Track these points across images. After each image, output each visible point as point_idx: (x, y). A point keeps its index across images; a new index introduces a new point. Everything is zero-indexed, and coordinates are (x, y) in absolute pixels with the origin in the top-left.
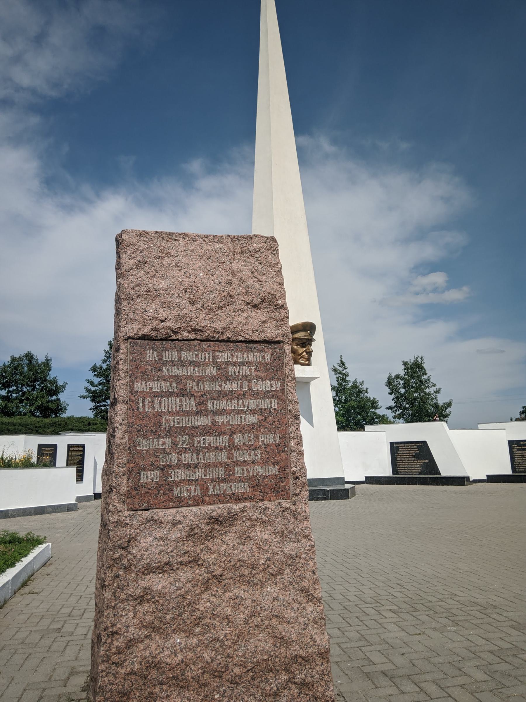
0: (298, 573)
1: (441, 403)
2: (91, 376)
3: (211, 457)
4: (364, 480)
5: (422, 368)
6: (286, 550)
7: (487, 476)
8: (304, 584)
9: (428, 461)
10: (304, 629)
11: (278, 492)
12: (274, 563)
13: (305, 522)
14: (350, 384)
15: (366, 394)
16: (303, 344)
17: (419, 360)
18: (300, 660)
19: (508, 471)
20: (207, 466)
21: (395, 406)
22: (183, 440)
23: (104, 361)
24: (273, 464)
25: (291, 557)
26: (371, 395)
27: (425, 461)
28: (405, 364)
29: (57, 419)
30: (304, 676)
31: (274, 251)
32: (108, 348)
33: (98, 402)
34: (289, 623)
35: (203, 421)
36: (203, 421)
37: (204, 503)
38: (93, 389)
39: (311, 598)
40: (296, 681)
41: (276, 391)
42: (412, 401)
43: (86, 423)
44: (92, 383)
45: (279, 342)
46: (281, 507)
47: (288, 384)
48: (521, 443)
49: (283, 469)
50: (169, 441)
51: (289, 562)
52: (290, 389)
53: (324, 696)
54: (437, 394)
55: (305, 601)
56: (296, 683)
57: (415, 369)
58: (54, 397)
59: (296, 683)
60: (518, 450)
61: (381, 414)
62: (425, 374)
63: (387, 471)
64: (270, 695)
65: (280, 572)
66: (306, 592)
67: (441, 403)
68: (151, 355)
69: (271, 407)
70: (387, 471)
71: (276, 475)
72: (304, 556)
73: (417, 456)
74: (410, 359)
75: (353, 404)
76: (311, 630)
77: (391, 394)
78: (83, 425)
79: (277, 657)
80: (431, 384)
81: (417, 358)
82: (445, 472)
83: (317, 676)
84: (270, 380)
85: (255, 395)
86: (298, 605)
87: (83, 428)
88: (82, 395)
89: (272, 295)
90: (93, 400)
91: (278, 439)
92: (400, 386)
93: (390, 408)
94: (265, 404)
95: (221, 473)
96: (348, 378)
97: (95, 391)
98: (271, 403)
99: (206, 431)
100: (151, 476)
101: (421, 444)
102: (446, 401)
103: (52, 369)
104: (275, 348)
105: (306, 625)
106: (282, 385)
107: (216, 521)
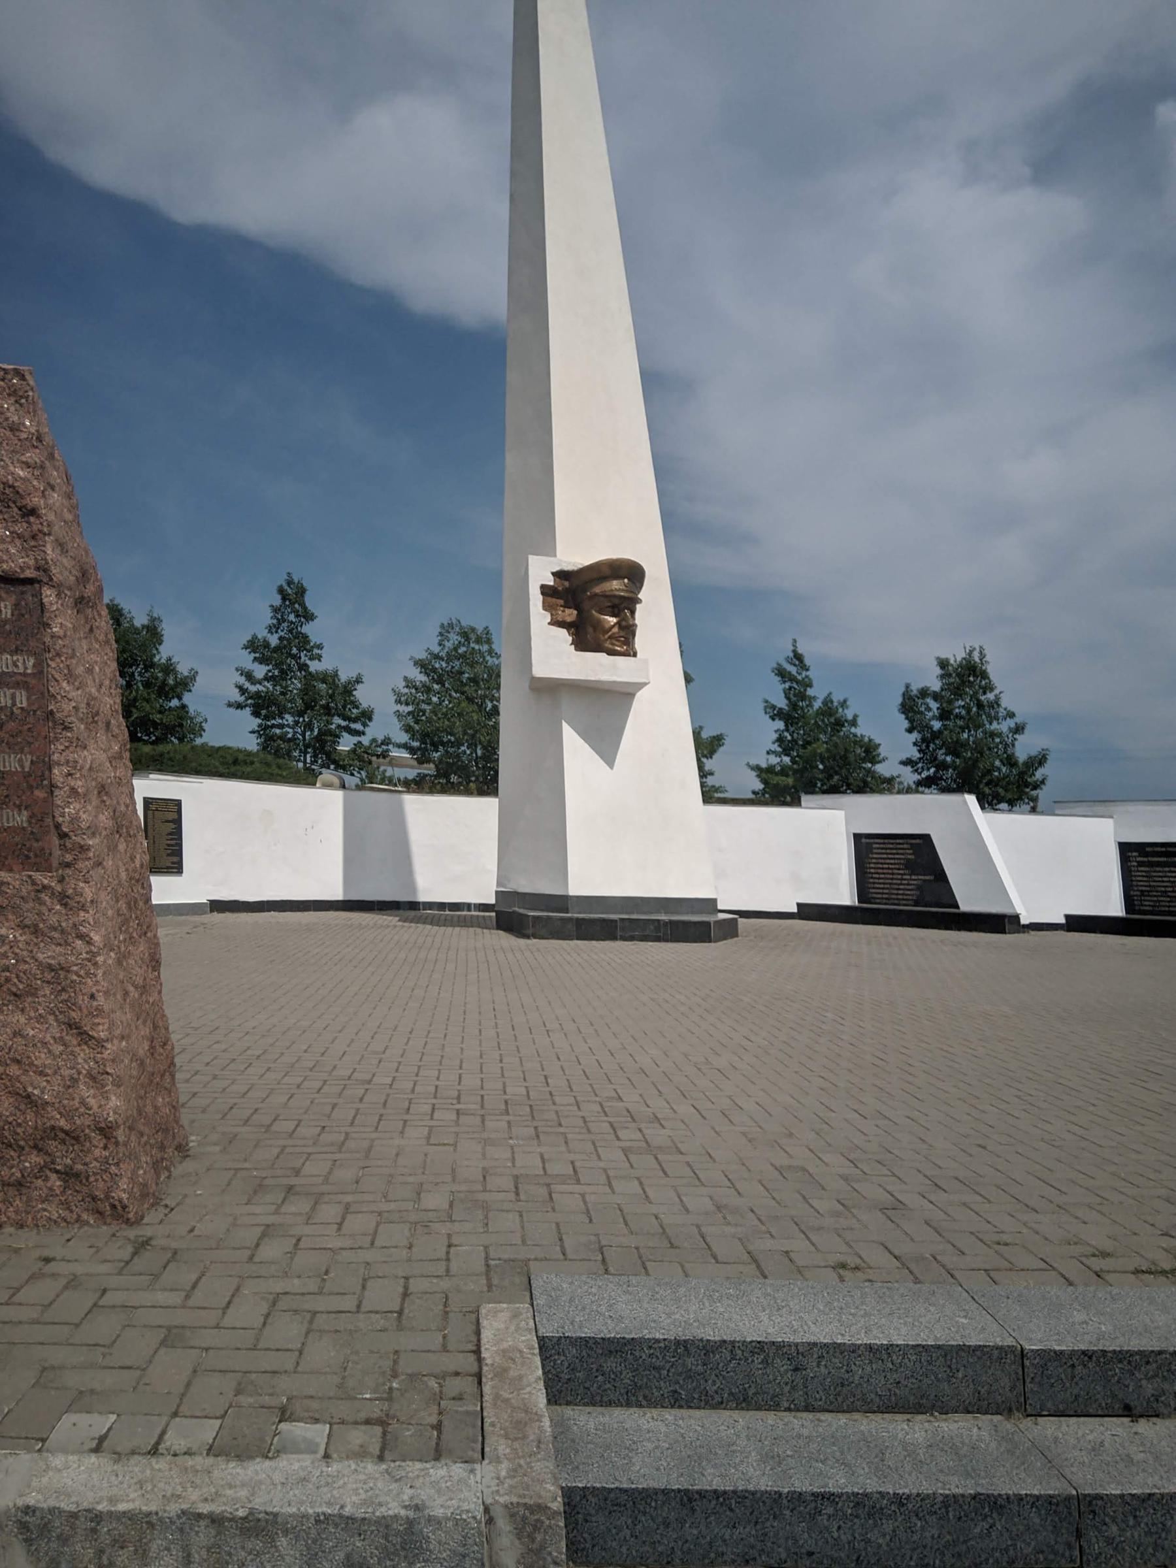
0: (64, 996)
1: (1021, 755)
2: (247, 660)
4: (795, 910)
5: (984, 675)
6: (40, 956)
7: (1067, 917)
8: (73, 1014)
9: (932, 878)
10: (69, 1087)
11: (28, 857)
12: (17, 976)
13: (82, 914)
14: (817, 705)
15: (853, 730)
16: (613, 607)
17: (976, 656)
18: (62, 1135)
19: (1115, 907)
21: (920, 759)
23: (272, 629)
24: (19, 807)
25: (50, 968)
26: (863, 730)
27: (927, 878)
28: (943, 664)
29: (186, 748)
30: (69, 1161)
31: (21, 397)
32: (277, 600)
33: (266, 718)
34: (42, 1074)
38: (253, 688)
39: (85, 1037)
40: (58, 1168)
41: (25, 675)
42: (955, 749)
43: (230, 759)
44: (249, 676)
45: (30, 581)
46: (34, 883)
47: (50, 662)
48: (1148, 849)
49: (38, 818)
51: (49, 976)
52: (54, 672)
53: (107, 1197)
54: (1017, 736)
55: (75, 1042)
56: (57, 1172)
57: (966, 677)
58: (175, 703)
59: (57, 1172)
60: (1140, 864)
61: (887, 775)
62: (989, 688)
63: (844, 894)
64: (9, 1185)
65: (32, 992)
66: (77, 1028)
67: (1021, 755)
69: (14, 704)
70: (844, 894)
71: (23, 828)
72: (75, 968)
73: (911, 867)
74: (956, 654)
75: (822, 749)
76: (84, 1090)
77: (910, 731)
78: (223, 763)
79: (19, 1125)
80: (1002, 713)
81: (971, 652)
82: (965, 906)
83: (95, 1164)
84: (12, 653)
86: (61, 1048)
87: (221, 769)
88: (232, 700)
89: (10, 487)
90: (256, 714)
91: (27, 765)
92: (931, 714)
93: (908, 762)
96: (810, 692)
97: (258, 693)
98: (13, 697)
101: (918, 841)
102: (1034, 753)
103: (165, 638)
104: (23, 593)
105: (74, 1081)
106: (39, 664)
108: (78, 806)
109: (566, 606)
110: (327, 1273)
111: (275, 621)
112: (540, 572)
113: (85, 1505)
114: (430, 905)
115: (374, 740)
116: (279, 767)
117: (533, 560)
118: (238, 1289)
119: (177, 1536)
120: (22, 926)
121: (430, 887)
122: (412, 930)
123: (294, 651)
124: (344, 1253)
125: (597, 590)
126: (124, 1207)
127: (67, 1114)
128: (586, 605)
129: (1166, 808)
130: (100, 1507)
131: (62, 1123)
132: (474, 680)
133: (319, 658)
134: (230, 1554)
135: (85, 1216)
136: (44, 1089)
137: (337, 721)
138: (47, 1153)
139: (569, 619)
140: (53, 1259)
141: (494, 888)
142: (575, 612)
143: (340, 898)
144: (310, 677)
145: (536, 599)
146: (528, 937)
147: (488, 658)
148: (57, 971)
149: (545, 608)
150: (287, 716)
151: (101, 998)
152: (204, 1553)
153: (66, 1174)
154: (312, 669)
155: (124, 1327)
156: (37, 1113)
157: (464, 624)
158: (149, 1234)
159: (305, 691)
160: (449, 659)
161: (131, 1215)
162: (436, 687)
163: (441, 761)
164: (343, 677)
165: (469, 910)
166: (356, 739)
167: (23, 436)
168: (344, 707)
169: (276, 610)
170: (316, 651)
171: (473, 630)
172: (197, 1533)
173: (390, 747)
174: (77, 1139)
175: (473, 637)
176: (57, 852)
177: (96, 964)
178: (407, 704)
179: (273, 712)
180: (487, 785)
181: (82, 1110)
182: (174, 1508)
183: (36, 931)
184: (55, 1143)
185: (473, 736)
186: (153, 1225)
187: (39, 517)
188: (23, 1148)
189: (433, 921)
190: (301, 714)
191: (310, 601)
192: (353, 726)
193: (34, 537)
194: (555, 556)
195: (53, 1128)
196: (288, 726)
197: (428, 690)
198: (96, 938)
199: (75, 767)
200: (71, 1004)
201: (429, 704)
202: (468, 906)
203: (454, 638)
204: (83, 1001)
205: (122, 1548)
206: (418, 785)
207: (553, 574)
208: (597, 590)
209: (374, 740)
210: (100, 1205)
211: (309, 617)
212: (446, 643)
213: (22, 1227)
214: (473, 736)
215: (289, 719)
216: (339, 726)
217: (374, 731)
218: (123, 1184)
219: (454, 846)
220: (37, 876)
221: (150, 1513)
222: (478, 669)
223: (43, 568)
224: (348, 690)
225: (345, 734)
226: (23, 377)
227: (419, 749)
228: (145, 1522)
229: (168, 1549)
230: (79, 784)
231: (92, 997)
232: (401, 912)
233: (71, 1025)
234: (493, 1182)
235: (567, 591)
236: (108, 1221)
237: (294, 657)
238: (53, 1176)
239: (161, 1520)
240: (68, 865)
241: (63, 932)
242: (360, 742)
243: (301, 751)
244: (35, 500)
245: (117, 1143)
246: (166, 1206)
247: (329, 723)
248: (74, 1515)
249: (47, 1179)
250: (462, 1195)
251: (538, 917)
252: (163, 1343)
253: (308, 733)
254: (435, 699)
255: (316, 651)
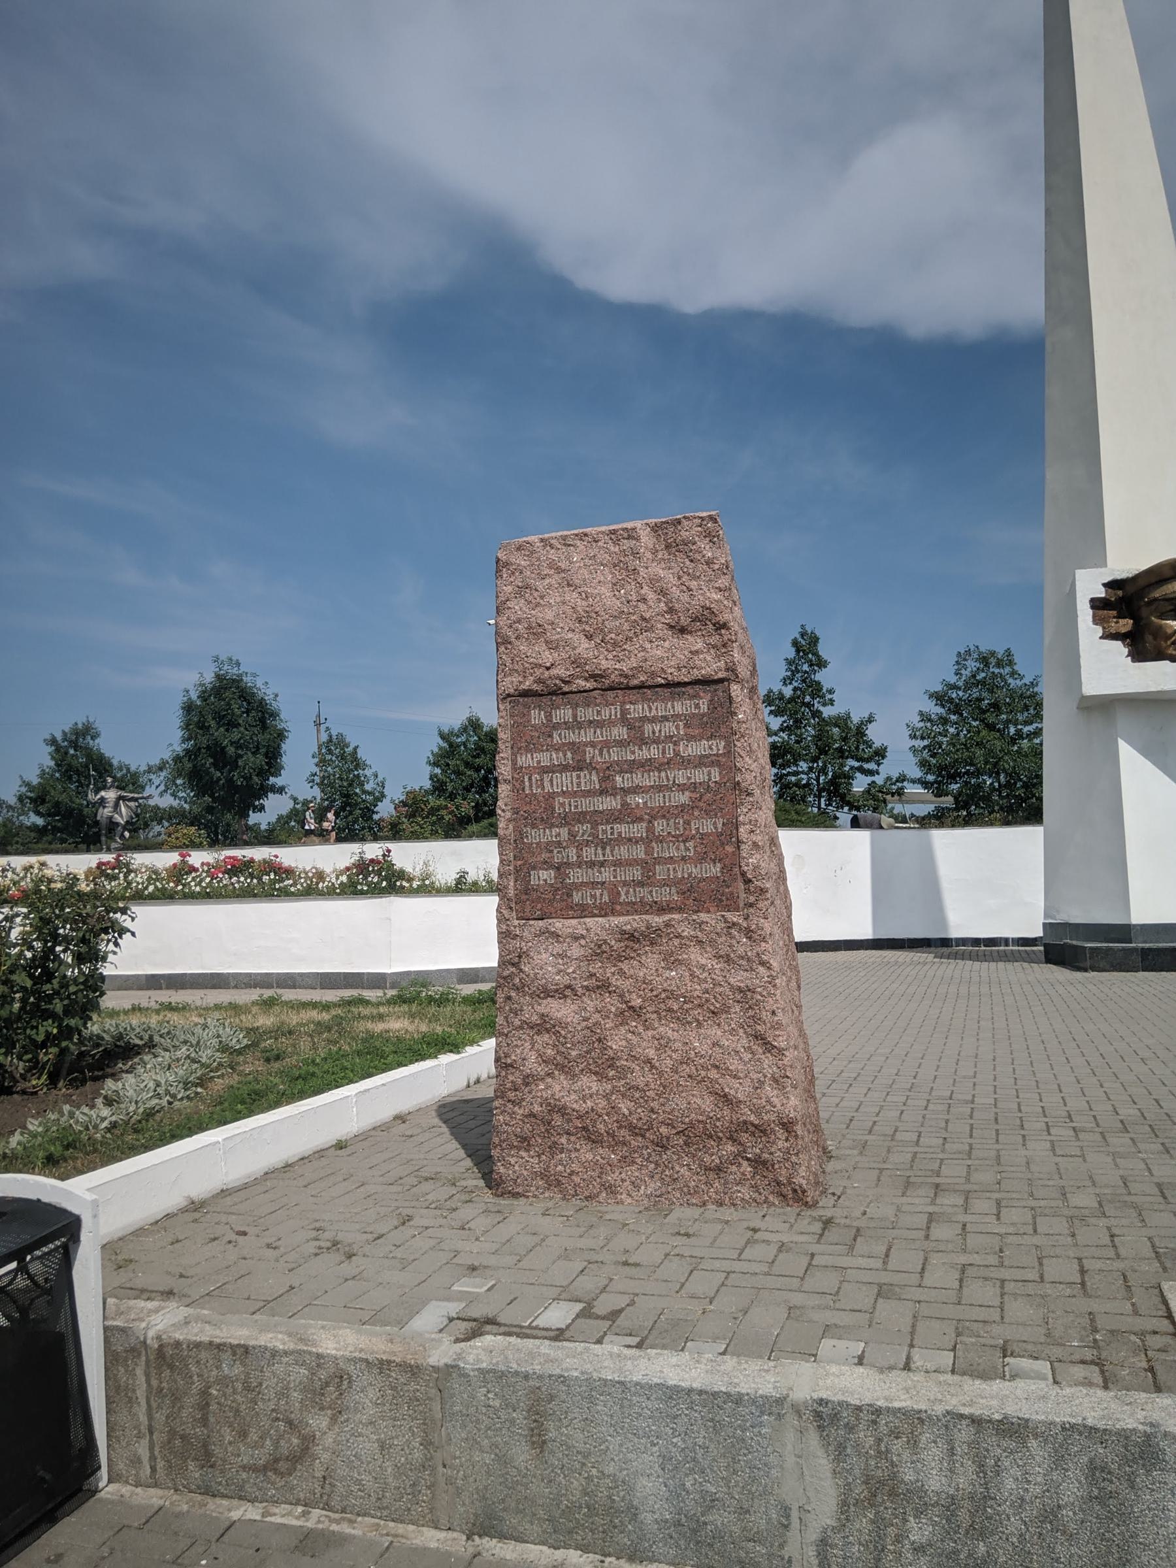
0: (751, 1013)
3: (623, 852)
6: (732, 980)
8: (758, 1027)
13: (763, 944)
18: (752, 1129)
20: (618, 863)
22: (583, 829)
23: (786, 681)
25: (740, 990)
32: (791, 653)
33: (783, 766)
34: (735, 1077)
35: (609, 803)
36: (609, 803)
37: (613, 913)
39: (768, 1047)
41: (717, 755)
45: (721, 681)
50: (564, 832)
53: (790, 1183)
56: (748, 1159)
59: (748, 1159)
65: (726, 1009)
68: (537, 717)
76: (769, 1090)
79: (718, 1119)
83: (779, 1153)
85: (686, 763)
91: (720, 826)
94: (699, 776)
95: (637, 873)
98: (709, 774)
99: (614, 817)
100: (546, 876)
104: (716, 690)
105: (761, 1083)
107: (631, 937)
108: (758, 856)
109: (1120, 616)
110: (1001, 1251)
111: (789, 673)
112: (1090, 584)
113: (867, 1401)
114: (963, 941)
115: (889, 779)
116: (797, 813)
117: (1080, 574)
118: (926, 1259)
119: (943, 1431)
120: (718, 957)
121: (962, 923)
122: (944, 966)
123: (808, 699)
124: (1011, 1237)
125: (1157, 594)
126: (804, 1192)
127: (757, 1111)
128: (1144, 612)
129: (72, 1519)
130: (879, 1403)
131: (752, 1118)
132: (995, 706)
133: (832, 702)
134: (987, 1450)
135: (771, 1198)
136: (739, 1090)
137: (852, 763)
138: (740, 1144)
139: (1123, 630)
140: (759, 1230)
141: (1042, 920)
142: (1131, 621)
143: (871, 937)
144: (824, 724)
145: (1085, 614)
146: (1086, 970)
147: (1010, 681)
148: (744, 993)
149: (1095, 622)
150: (801, 763)
151: (780, 1013)
152: (965, 1446)
153: (756, 1161)
154: (825, 715)
155: (841, 1282)
156: (732, 1110)
157: (982, 649)
158: (829, 1215)
159: (817, 738)
160: (968, 686)
161: (809, 1199)
162: (953, 717)
163: (960, 793)
164: (856, 719)
165: (1007, 945)
166: (869, 779)
167: (716, 567)
168: (857, 748)
169: (790, 662)
170: (828, 696)
171: (993, 654)
172: (960, 1430)
173: (905, 784)
174: (764, 1132)
175: (993, 661)
176: (743, 895)
177: (775, 986)
178: (923, 738)
179: (789, 761)
180: (1034, 815)
181: (768, 1107)
182: (939, 1409)
183: (728, 960)
184: (747, 1135)
185: (995, 765)
186: (826, 1207)
187: (728, 629)
188: (721, 1139)
189: (971, 957)
190: (815, 760)
191: (823, 650)
192: (866, 766)
193: (724, 646)
194: (1106, 566)
195: (745, 1122)
196: (803, 772)
197: (944, 721)
198: (775, 964)
199: (755, 826)
200: (756, 1019)
201: (946, 736)
202: (1006, 941)
203: (972, 665)
204: (766, 1015)
205: (897, 1438)
206: (939, 819)
207: (1105, 585)
208: (1157, 594)
209: (889, 779)
210: (784, 1191)
211: (821, 664)
212: (963, 672)
213: (721, 1205)
214: (995, 765)
215: (803, 766)
216: (852, 768)
217: (888, 769)
218: (802, 1171)
219: (992, 879)
220: (728, 915)
221: (920, 1411)
222: (1000, 694)
223: (732, 669)
224: (860, 732)
225: (858, 775)
226: (715, 521)
227: (936, 782)
228: (917, 1418)
229: (935, 1442)
230: (758, 838)
231: (773, 1013)
232: (932, 949)
233: (757, 1037)
234: (1135, 1187)
235: (1121, 600)
236: (791, 1202)
237: (808, 705)
238: (745, 1163)
239: (929, 1417)
240: (751, 905)
241: (748, 960)
242: (873, 782)
243: (815, 796)
244: (725, 617)
245: (796, 1136)
246: (834, 1194)
247: (842, 765)
248: (859, 1408)
249: (740, 1165)
250: (1109, 1197)
251: (1097, 948)
252: (879, 1295)
253: (822, 778)
254: (952, 730)
255: (828, 696)
